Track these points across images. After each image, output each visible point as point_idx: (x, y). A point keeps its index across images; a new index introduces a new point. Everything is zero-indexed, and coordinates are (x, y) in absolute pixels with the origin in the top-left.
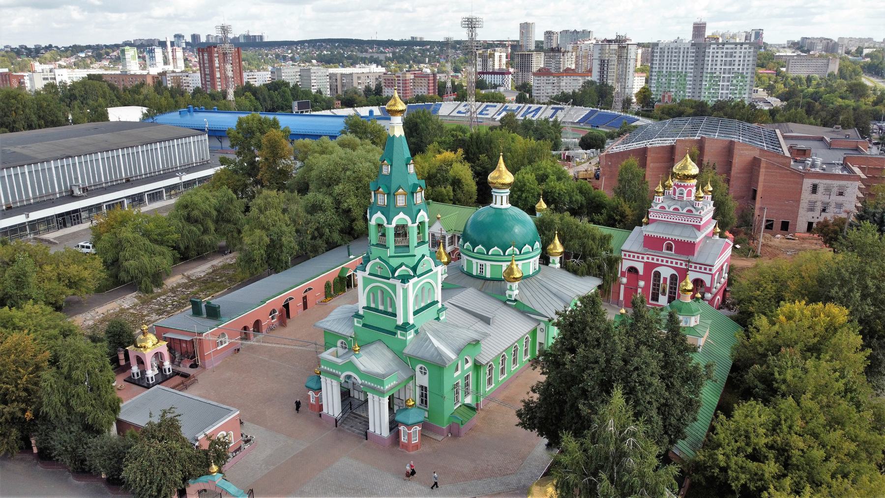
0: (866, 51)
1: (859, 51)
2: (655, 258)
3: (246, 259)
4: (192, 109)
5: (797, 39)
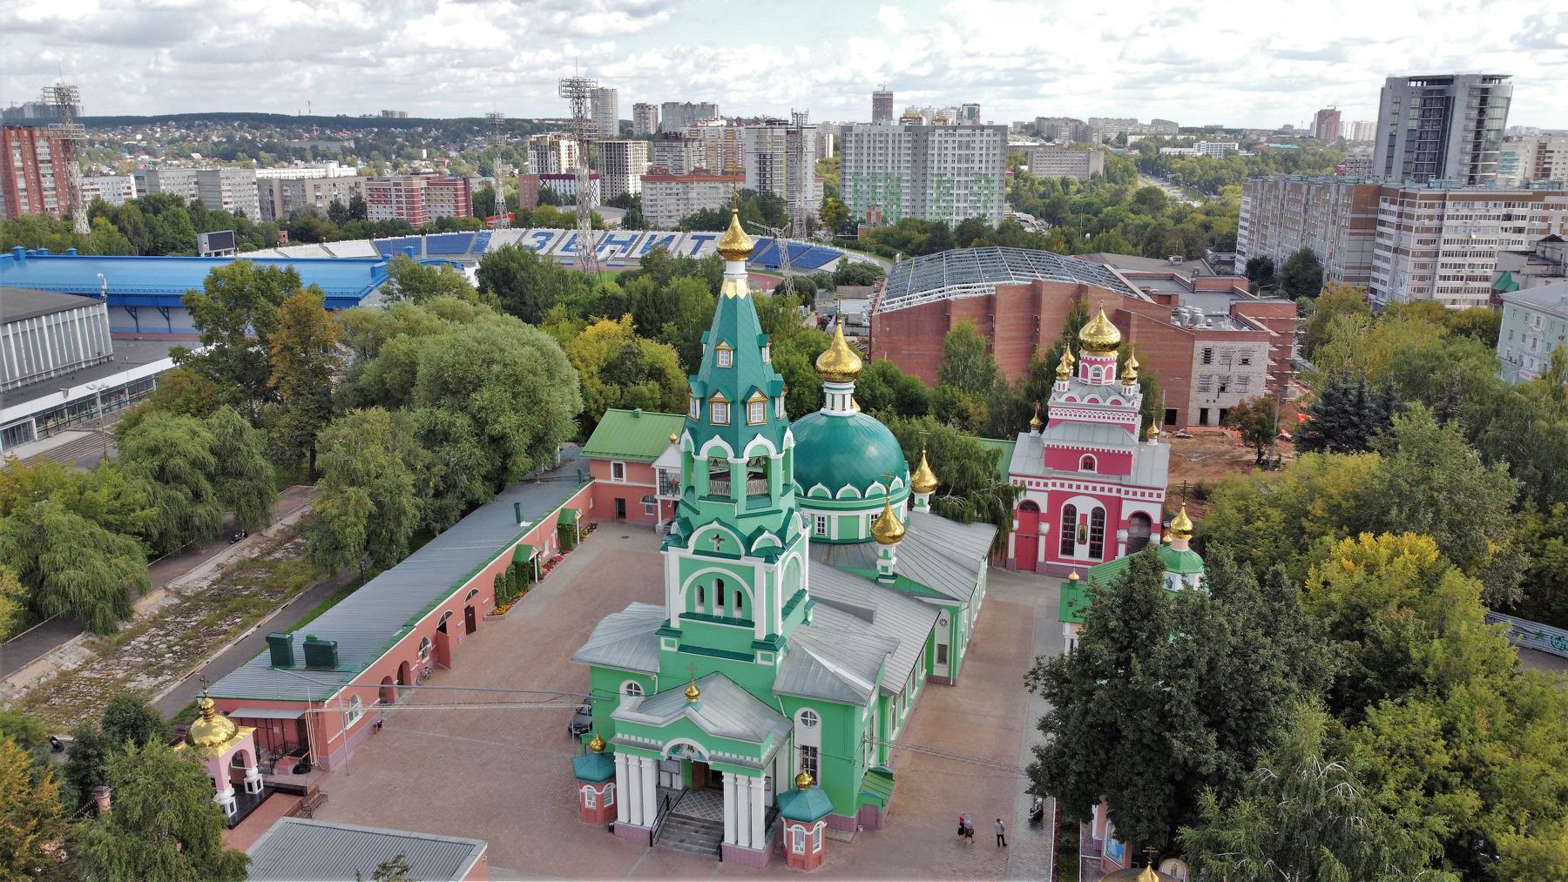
0: (1131, 139)
1: (1122, 139)
2: (1067, 483)
3: (327, 543)
4: (22, 254)
5: (1029, 118)
